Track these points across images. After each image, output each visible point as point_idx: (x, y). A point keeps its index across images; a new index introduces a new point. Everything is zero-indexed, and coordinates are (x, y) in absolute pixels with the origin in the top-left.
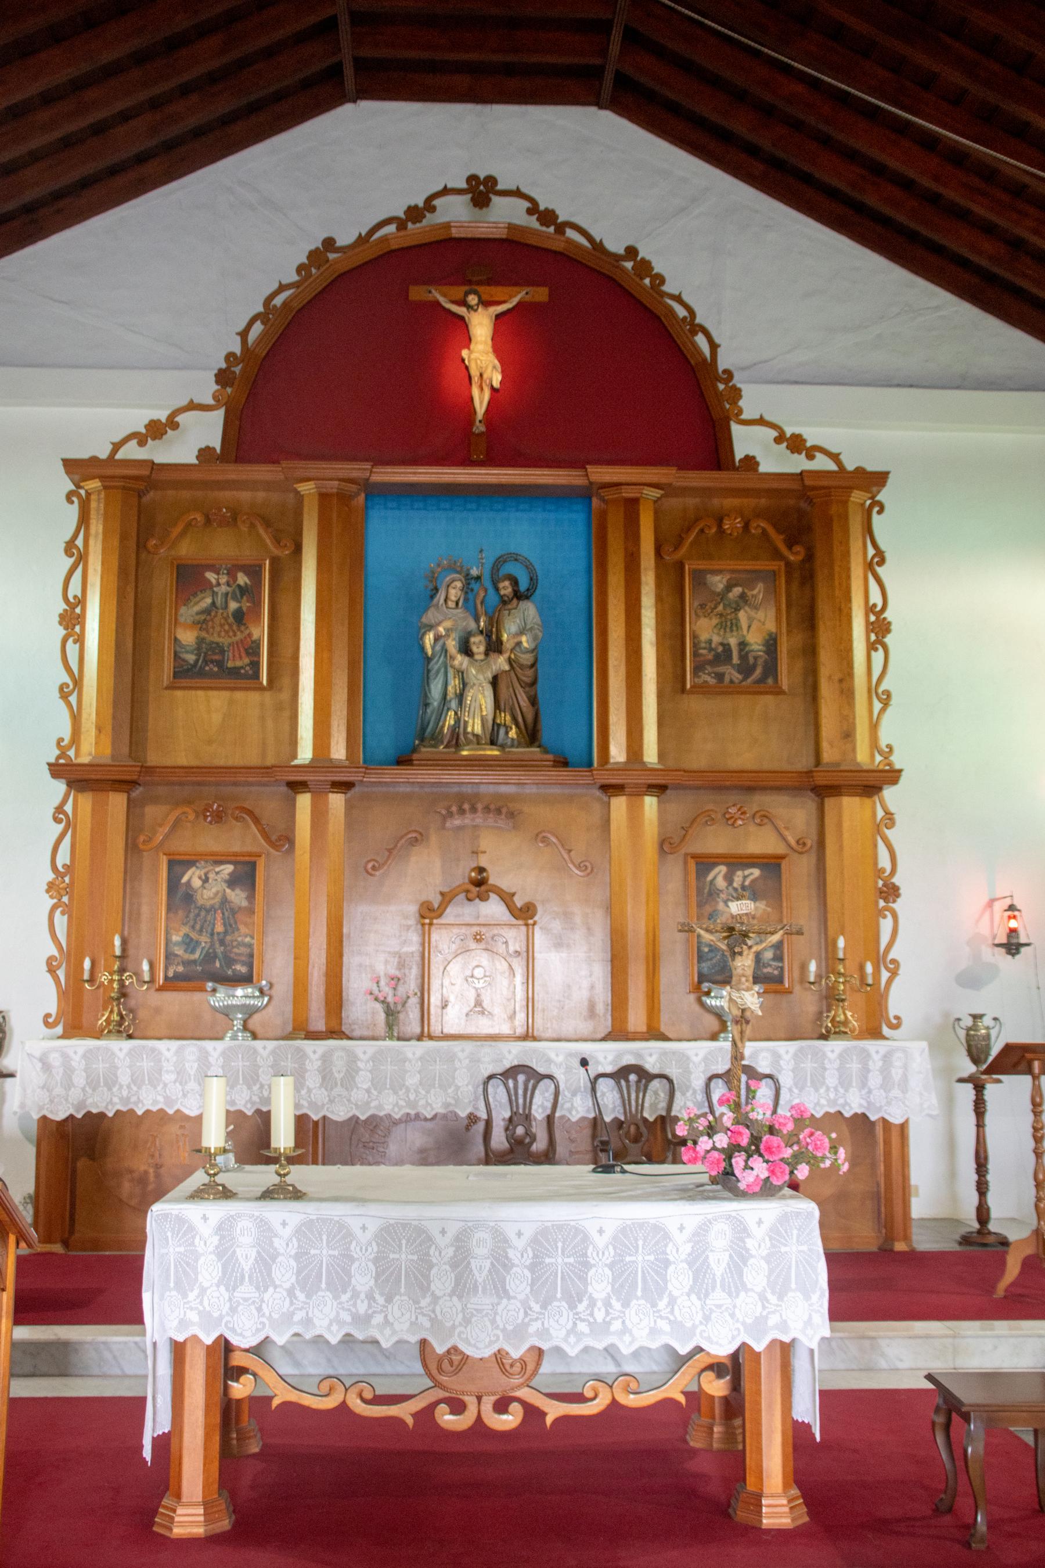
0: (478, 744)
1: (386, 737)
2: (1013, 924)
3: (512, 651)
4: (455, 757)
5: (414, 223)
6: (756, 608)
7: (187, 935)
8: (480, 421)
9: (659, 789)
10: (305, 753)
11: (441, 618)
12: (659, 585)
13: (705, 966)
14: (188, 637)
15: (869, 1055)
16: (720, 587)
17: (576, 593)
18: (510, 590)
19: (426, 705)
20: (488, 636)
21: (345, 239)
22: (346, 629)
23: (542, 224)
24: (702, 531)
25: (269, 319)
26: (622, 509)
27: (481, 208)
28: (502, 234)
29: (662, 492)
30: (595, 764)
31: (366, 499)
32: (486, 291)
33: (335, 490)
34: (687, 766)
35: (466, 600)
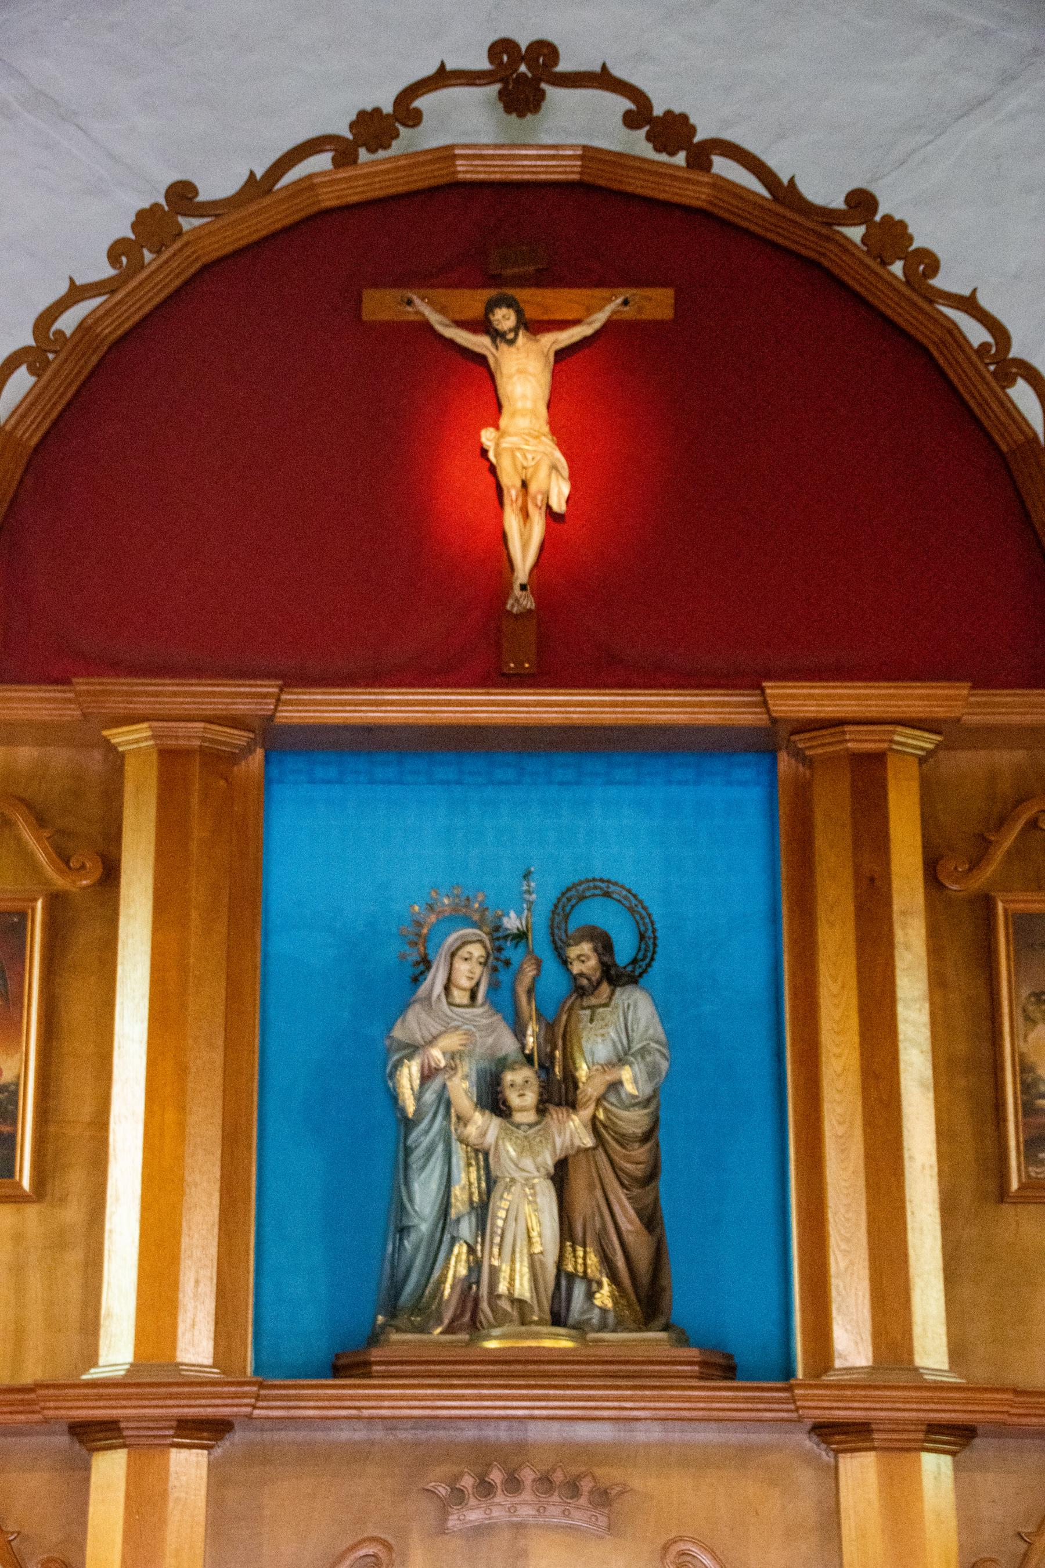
0: (523, 1323)
1: (309, 1319)
3: (598, 1102)
4: (471, 1354)
5: (372, 150)
8: (523, 587)
9: (956, 1436)
10: (117, 1351)
11: (435, 1028)
12: (935, 951)
17: (744, 964)
18: (593, 962)
19: (403, 1231)
20: (545, 1068)
21: (217, 184)
22: (218, 1057)
23: (657, 150)
25: (48, 362)
27: (521, 115)
28: (569, 171)
29: (939, 738)
30: (800, 1375)
31: (267, 759)
32: (539, 300)
33: (197, 743)
34: (1019, 1377)
35: (494, 986)
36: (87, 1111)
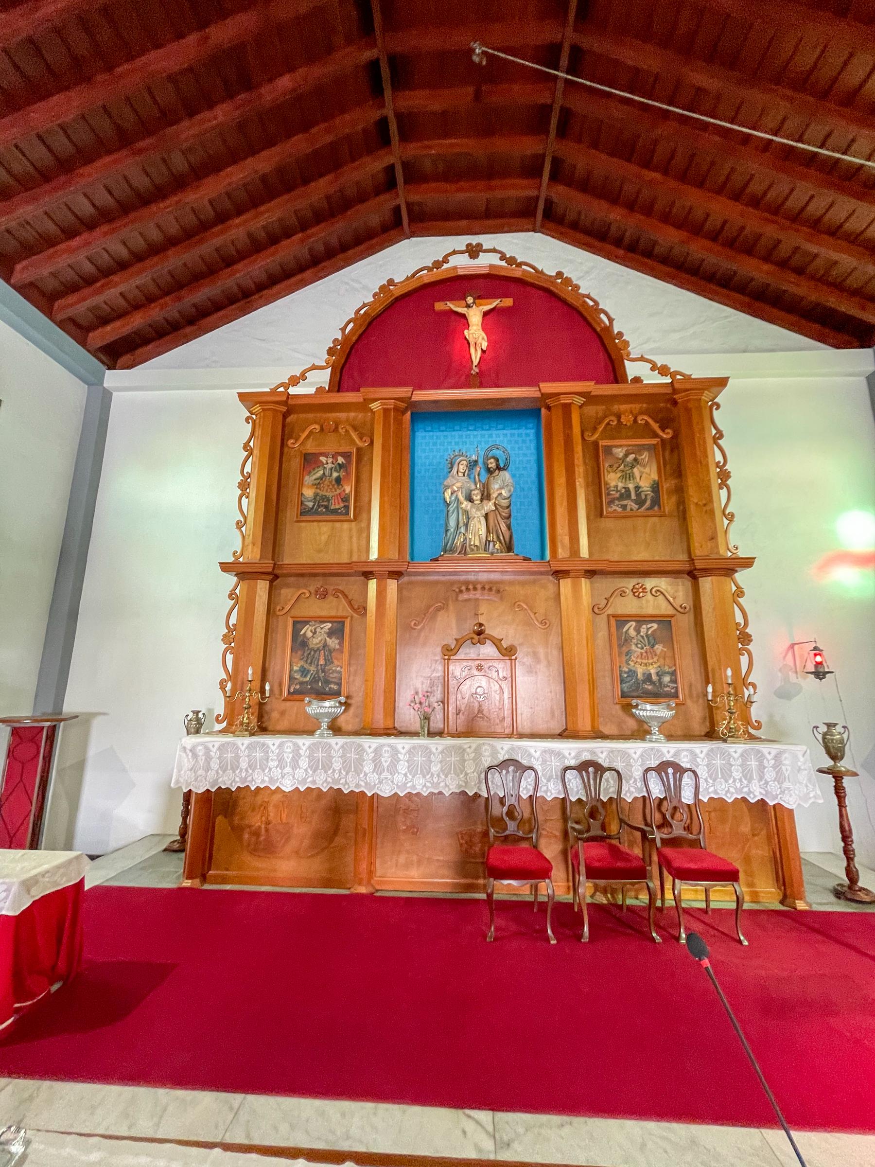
2: (818, 659)
6: (644, 466)
7: (302, 667)
9: (591, 574)
10: (374, 555)
13: (625, 687)
14: (308, 493)
15: (763, 755)
16: (621, 455)
19: (447, 531)
24: (608, 424)
26: (561, 411)
28: (485, 271)
36: (367, 499)
